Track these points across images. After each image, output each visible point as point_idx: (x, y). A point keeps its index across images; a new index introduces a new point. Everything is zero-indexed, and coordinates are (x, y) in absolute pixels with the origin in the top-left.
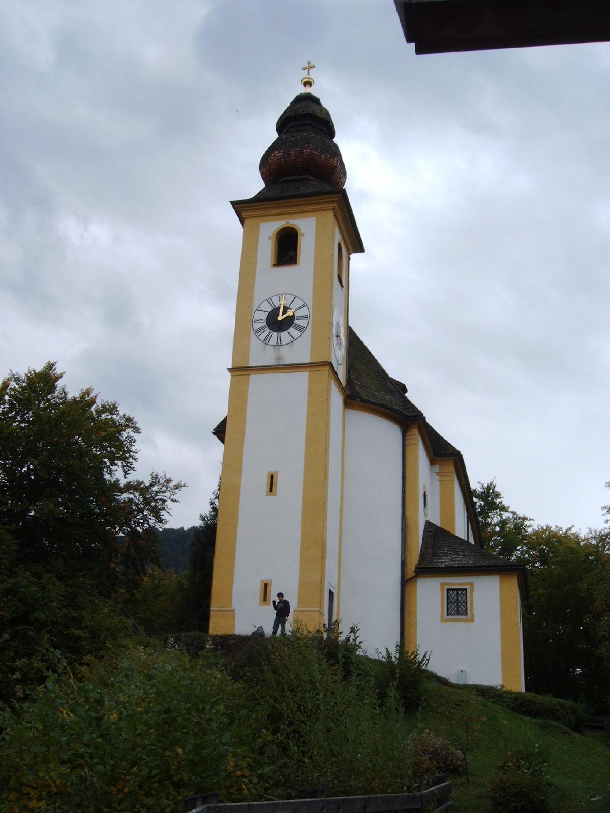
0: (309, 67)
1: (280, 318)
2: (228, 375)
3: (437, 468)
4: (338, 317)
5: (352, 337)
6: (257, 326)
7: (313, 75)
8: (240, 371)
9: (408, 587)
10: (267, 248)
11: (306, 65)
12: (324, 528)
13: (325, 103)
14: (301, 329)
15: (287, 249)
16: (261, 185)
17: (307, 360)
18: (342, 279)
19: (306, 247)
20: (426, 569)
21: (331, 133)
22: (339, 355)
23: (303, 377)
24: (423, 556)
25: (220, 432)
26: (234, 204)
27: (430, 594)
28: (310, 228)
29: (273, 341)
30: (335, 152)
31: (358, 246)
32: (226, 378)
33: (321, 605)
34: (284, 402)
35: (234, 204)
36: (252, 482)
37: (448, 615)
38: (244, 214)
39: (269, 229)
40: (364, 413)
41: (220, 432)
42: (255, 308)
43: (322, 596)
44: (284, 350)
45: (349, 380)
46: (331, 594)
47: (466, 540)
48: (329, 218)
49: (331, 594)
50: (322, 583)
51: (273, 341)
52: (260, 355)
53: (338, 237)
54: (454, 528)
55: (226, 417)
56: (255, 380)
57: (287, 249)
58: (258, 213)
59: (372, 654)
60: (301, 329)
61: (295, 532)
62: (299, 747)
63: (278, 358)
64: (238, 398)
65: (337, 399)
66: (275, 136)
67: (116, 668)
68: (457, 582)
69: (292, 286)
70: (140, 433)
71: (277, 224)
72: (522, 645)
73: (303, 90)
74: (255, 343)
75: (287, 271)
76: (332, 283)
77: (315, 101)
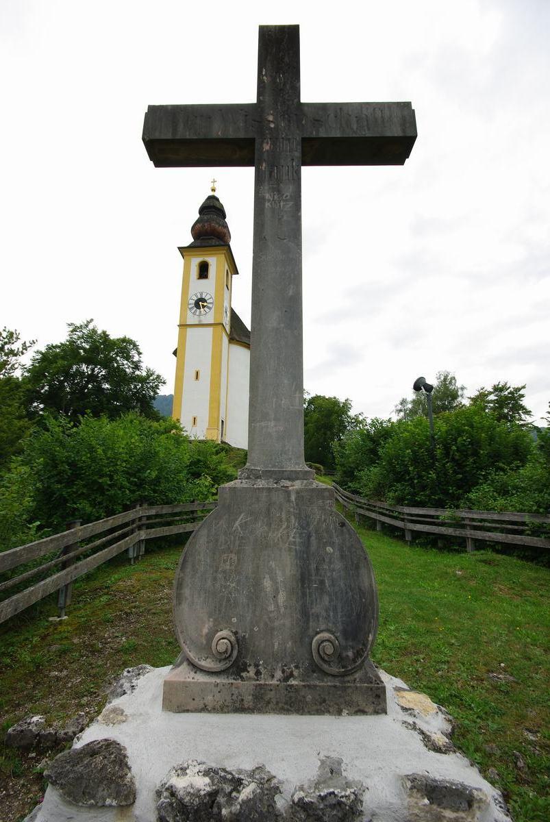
0: (214, 181)
1: (200, 303)
2: (178, 328)
4: (226, 304)
5: (232, 310)
6: (190, 306)
7: (216, 185)
8: (183, 326)
10: (195, 270)
11: (236, 83)
12: (219, 394)
13: (221, 201)
14: (210, 308)
15: (203, 271)
16: (192, 240)
17: (212, 322)
18: (229, 287)
19: (212, 271)
21: (224, 217)
22: (226, 320)
23: (211, 329)
25: (175, 353)
26: (179, 248)
28: (215, 262)
29: (198, 313)
30: (226, 226)
31: (236, 272)
32: (176, 331)
33: (218, 427)
34: (202, 340)
35: (179, 248)
36: (189, 374)
38: (184, 254)
39: (195, 262)
40: (238, 347)
41: (175, 353)
43: (218, 423)
44: (202, 318)
45: (231, 332)
46: (222, 421)
48: (222, 258)
49: (222, 421)
50: (218, 417)
51: (198, 313)
52: (192, 319)
53: (226, 267)
55: (176, 349)
56: (189, 330)
57: (203, 271)
58: (193, 253)
59: (112, 338)
60: (210, 308)
61: (206, 397)
63: (200, 321)
64: (182, 339)
65: (225, 340)
66: (198, 216)
69: (207, 288)
71: (200, 259)
72: (517, 536)
73: (211, 193)
74: (189, 314)
75: (203, 281)
76: (223, 288)
77: (217, 200)
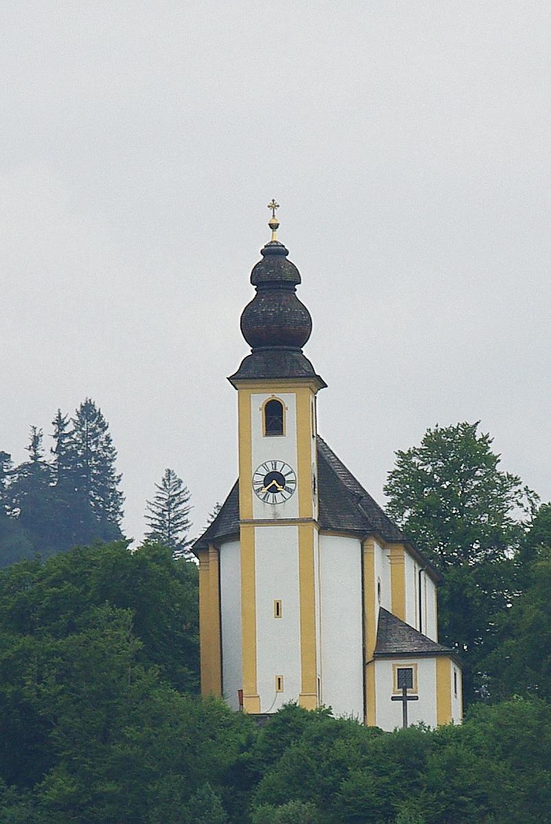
3: (388, 552)
6: (257, 487)
9: (369, 669)
14: (291, 491)
15: (274, 419)
16: (247, 350)
17: (297, 517)
20: (382, 654)
23: (295, 529)
24: (379, 641)
27: (385, 672)
37: (398, 669)
39: (259, 400)
42: (253, 472)
47: (418, 630)
54: (405, 620)
60: (291, 491)
62: (128, 590)
63: (275, 514)
67: (20, 543)
68: (404, 663)
70: (88, 411)
